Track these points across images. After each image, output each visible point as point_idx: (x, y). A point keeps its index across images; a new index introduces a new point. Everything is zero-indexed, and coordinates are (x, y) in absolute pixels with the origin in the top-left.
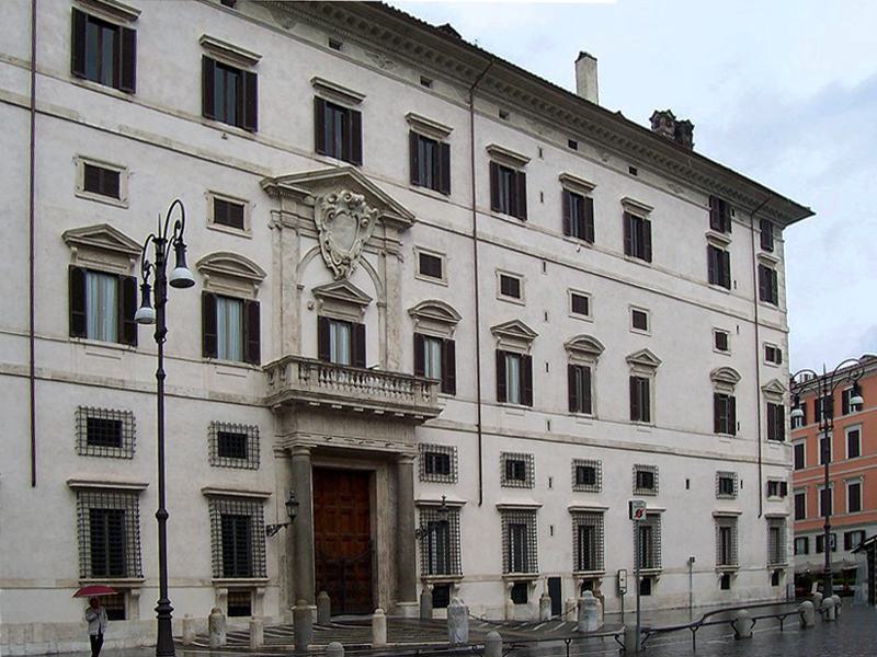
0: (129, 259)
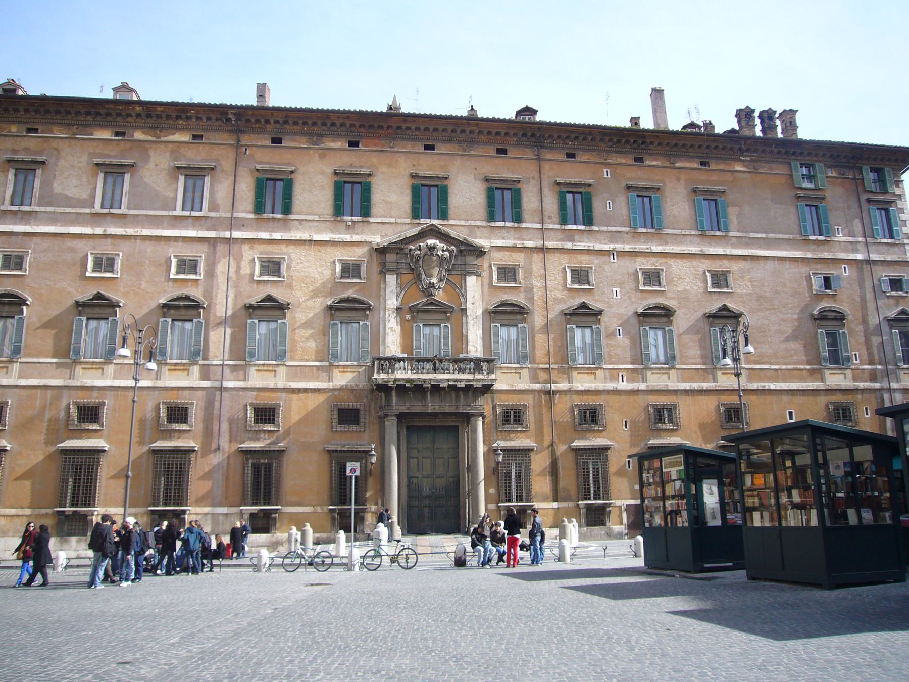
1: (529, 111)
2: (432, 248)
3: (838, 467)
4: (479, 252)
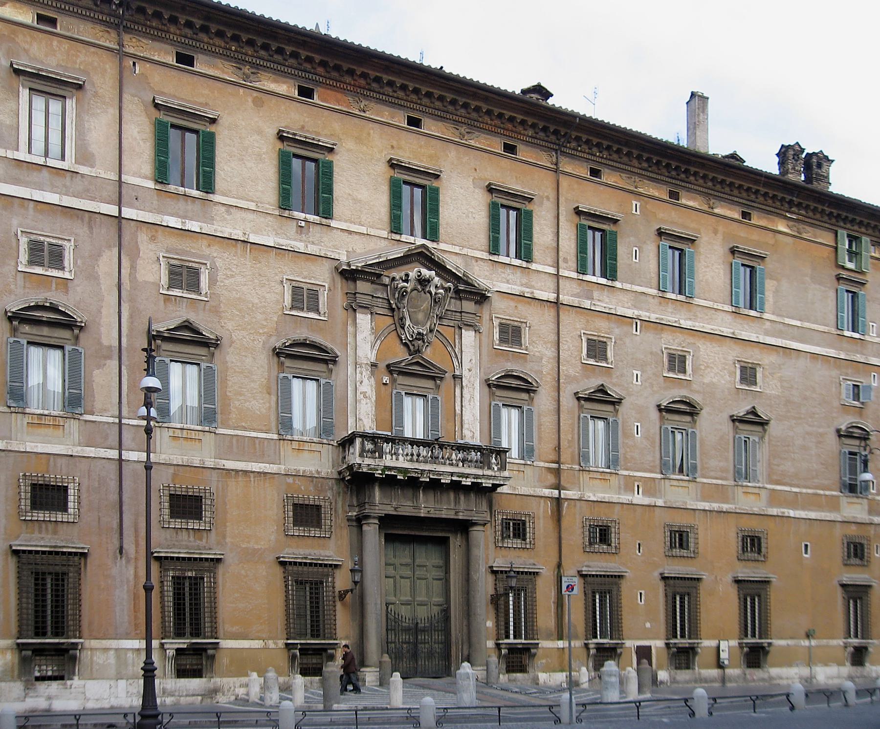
0: (209, 347)
1: (541, 91)
2: (423, 282)
3: (286, 689)
4: (481, 297)
